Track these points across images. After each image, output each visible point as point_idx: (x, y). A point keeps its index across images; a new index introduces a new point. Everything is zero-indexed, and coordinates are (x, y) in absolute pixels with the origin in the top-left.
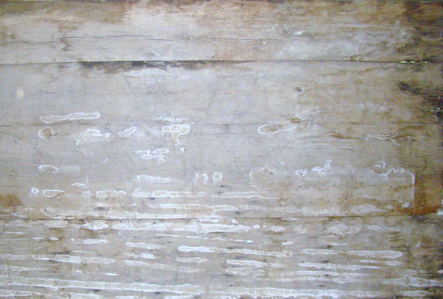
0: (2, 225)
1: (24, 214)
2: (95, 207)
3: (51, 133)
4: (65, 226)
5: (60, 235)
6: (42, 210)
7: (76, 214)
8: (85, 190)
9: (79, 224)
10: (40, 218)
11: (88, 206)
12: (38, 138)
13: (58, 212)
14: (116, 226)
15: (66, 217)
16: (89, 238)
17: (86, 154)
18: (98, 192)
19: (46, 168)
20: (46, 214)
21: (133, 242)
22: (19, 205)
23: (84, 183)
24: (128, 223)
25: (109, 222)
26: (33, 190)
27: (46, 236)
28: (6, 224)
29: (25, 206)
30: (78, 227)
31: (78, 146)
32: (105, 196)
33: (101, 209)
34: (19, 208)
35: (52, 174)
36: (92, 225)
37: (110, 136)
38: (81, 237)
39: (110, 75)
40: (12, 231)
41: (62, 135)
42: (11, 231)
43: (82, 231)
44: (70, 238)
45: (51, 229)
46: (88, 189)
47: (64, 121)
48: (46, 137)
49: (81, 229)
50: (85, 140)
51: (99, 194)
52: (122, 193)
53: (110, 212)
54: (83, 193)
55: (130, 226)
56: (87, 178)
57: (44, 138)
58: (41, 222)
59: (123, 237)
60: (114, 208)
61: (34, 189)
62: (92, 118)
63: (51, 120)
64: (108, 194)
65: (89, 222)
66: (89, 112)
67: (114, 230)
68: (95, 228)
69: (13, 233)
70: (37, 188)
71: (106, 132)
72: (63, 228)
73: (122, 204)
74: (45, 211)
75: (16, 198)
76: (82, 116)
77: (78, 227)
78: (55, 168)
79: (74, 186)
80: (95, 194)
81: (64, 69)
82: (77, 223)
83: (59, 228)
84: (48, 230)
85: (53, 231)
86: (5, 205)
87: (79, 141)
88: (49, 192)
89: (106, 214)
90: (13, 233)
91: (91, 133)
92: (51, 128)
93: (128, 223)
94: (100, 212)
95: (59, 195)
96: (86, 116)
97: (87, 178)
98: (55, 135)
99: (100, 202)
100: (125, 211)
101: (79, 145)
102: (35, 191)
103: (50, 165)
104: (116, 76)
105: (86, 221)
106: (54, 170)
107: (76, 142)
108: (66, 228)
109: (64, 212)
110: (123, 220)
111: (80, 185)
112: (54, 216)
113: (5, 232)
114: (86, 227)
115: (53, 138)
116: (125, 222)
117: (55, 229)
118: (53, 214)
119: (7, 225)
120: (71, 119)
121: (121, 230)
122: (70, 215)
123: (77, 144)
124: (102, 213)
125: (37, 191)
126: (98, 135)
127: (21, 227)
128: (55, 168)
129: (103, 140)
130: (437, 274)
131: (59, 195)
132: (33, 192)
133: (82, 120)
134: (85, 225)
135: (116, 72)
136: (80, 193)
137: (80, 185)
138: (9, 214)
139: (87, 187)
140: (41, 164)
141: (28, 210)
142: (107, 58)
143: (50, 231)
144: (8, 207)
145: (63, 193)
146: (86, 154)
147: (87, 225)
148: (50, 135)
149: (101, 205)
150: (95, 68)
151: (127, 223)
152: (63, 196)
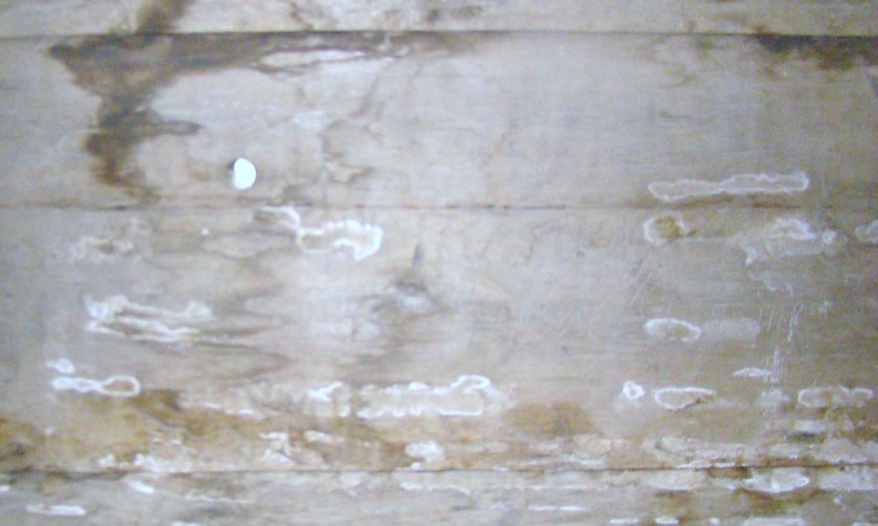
0: (522, 488)
1: (595, 457)
2: (791, 433)
3: (677, 229)
4: (695, 486)
5: (682, 511)
6: (648, 445)
7: (740, 453)
8: (768, 387)
9: (734, 478)
10: (631, 466)
11: (773, 432)
12: (642, 242)
13: (692, 450)
14: (828, 481)
15: (712, 461)
16: (757, 515)
17: (772, 289)
18: (801, 393)
19: (664, 328)
20: (659, 456)
21: (871, 522)
22: (583, 432)
23: (769, 368)
24: (859, 471)
25: (812, 471)
26: (626, 390)
27: (645, 515)
28: (534, 484)
29: (601, 435)
30: (731, 486)
31: (751, 267)
32: (818, 403)
33: (806, 437)
34: (582, 439)
35: (683, 344)
36: (768, 481)
37: (837, 239)
38: (736, 514)
39: (833, 73)
40: (552, 504)
41: (707, 236)
42: (546, 504)
43: (742, 496)
44: (708, 517)
45: (661, 494)
46: (776, 385)
47: (715, 196)
48: (664, 241)
49: (738, 491)
50: (769, 249)
51: (804, 397)
52: (862, 394)
53: (830, 444)
54: (764, 394)
55: (863, 479)
56: (777, 353)
57: (659, 242)
58: (634, 476)
59: (844, 508)
60: (839, 434)
61: (629, 386)
62: (787, 190)
63: (680, 193)
64: (827, 395)
65: (760, 473)
66: (782, 173)
67: (824, 492)
68: (775, 487)
69: (553, 508)
70: (638, 383)
71: (823, 229)
72: (691, 493)
73: (861, 423)
74: (658, 446)
75: (577, 412)
76: (765, 184)
77: (731, 486)
78: (690, 326)
79: (740, 378)
80: (794, 396)
81: (709, 52)
82: (729, 477)
83: (682, 492)
84: (652, 499)
85: (666, 500)
86: (544, 431)
87: (754, 251)
88: (671, 393)
89: (818, 450)
90: (553, 508)
91: (785, 230)
92: (678, 215)
93: (859, 471)
94: (804, 445)
95: (698, 402)
96: (774, 185)
97: (777, 353)
98: (692, 234)
99: (803, 418)
100: (866, 440)
101: (755, 262)
102: (633, 393)
103: (679, 318)
104: (848, 75)
105: (754, 472)
106: (687, 332)
107: (745, 256)
108: (699, 490)
109: (709, 448)
110: (850, 465)
111: (755, 372)
112: (682, 459)
113: (530, 507)
114: (751, 485)
115: (684, 242)
116: (852, 469)
117: (671, 494)
118: (678, 454)
119: (537, 488)
120: (733, 191)
121: (840, 492)
122: (724, 455)
123: (749, 261)
124: (808, 449)
125: (640, 391)
126: (802, 238)
127: (578, 492)
128: (690, 326)
129: (816, 251)
130: (562, 435)
131: (698, 402)
132: (628, 396)
133: (762, 194)
134: (749, 481)
135: (848, 67)
136: (753, 397)
137: (755, 372)
138: (556, 456)
139: (773, 380)
140: (651, 316)
141: (612, 445)
142: (830, 28)
143: (657, 500)
144: (552, 438)
145: (709, 398)
146: (772, 289)
147: (756, 481)
148: (675, 235)
149: (806, 426)
150: (795, 52)
151: (856, 470)
152: (710, 406)
